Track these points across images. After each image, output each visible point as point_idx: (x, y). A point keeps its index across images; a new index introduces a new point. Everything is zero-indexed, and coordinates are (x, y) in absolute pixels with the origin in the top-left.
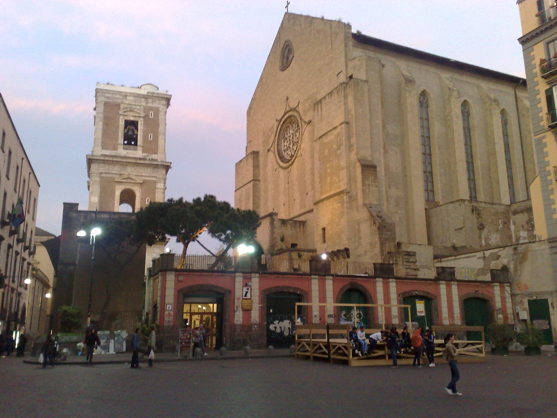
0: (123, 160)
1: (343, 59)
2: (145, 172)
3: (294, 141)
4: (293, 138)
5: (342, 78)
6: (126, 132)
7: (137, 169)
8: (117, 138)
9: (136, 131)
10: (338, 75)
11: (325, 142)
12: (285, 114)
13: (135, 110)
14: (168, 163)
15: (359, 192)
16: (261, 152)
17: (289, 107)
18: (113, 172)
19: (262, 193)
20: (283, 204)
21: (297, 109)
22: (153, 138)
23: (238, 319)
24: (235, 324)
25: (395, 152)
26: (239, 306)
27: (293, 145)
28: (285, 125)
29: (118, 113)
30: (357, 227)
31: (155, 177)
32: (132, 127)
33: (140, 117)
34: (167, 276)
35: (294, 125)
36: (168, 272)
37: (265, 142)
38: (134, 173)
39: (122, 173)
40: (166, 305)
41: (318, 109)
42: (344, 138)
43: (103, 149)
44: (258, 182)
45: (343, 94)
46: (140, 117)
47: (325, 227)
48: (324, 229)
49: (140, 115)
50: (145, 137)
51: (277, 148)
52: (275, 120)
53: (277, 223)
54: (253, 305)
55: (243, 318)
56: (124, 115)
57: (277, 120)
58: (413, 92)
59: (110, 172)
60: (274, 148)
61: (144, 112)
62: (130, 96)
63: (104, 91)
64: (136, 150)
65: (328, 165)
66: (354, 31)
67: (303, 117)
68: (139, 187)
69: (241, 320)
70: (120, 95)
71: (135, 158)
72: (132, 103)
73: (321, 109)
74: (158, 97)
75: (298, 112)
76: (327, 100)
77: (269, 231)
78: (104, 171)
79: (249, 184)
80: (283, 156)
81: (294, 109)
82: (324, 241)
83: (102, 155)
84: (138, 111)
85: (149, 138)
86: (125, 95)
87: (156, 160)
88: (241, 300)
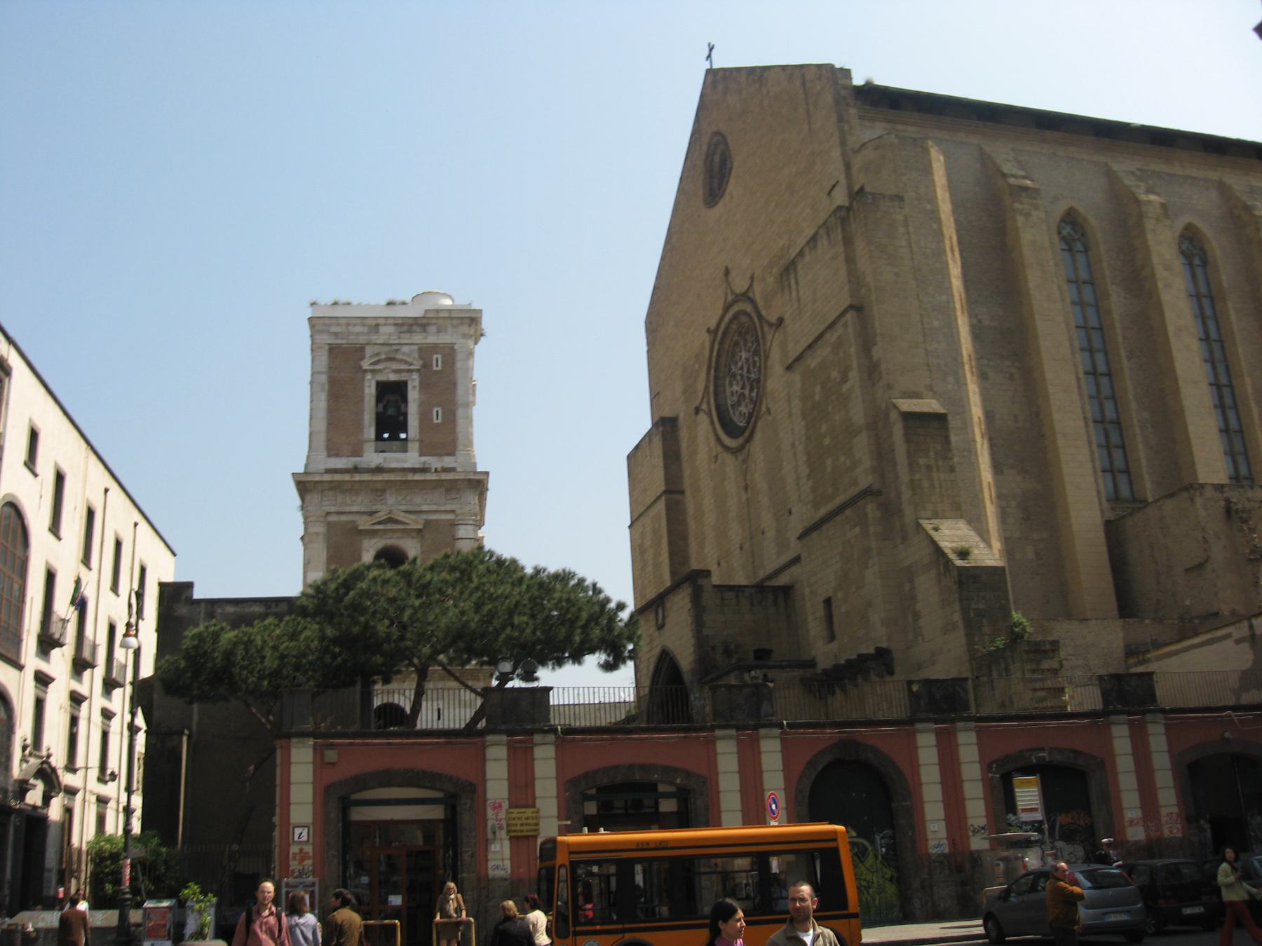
0: (375, 478)
1: (836, 153)
2: (428, 502)
3: (753, 376)
4: (748, 371)
5: (841, 197)
6: (381, 409)
7: (408, 498)
8: (359, 427)
9: (403, 406)
10: (830, 193)
11: (812, 367)
12: (726, 309)
13: (399, 356)
14: (481, 473)
15: (903, 489)
16: (682, 415)
17: (733, 292)
18: (355, 509)
19: (692, 524)
20: (738, 546)
21: (750, 294)
22: (443, 419)
23: (499, 863)
24: (490, 877)
25: (1007, 375)
26: (501, 828)
27: (751, 390)
28: (728, 341)
29: (361, 367)
30: (907, 587)
31: (453, 511)
32: (393, 398)
33: (410, 371)
34: (294, 751)
35: (748, 337)
36: (294, 740)
37: (688, 390)
38: (403, 508)
39: (374, 508)
40: (291, 830)
41: (789, 284)
42: (853, 350)
43: (329, 456)
44: (678, 497)
45: (840, 236)
46: (410, 371)
47: (830, 595)
48: (828, 602)
49: (412, 367)
50: (425, 416)
51: (716, 401)
52: (705, 329)
53: (708, 599)
54: (541, 824)
55: (511, 859)
56: (373, 371)
57: (708, 331)
58: (1035, 213)
59: (348, 509)
60: (709, 403)
61: (421, 357)
62: (385, 325)
63: (327, 321)
64: (405, 450)
65: (824, 428)
66: (858, 80)
67: (764, 313)
68: (416, 540)
69: (508, 864)
70: (364, 325)
71: (403, 470)
72: (392, 342)
73: (797, 283)
74: (452, 318)
75: (752, 301)
76: (808, 258)
77: (690, 621)
78: (333, 509)
79: (658, 503)
80: (731, 420)
81: (746, 296)
82: (832, 637)
83: (328, 471)
84: (405, 358)
85: (432, 417)
86: (374, 325)
87: (453, 470)
88: (504, 811)
